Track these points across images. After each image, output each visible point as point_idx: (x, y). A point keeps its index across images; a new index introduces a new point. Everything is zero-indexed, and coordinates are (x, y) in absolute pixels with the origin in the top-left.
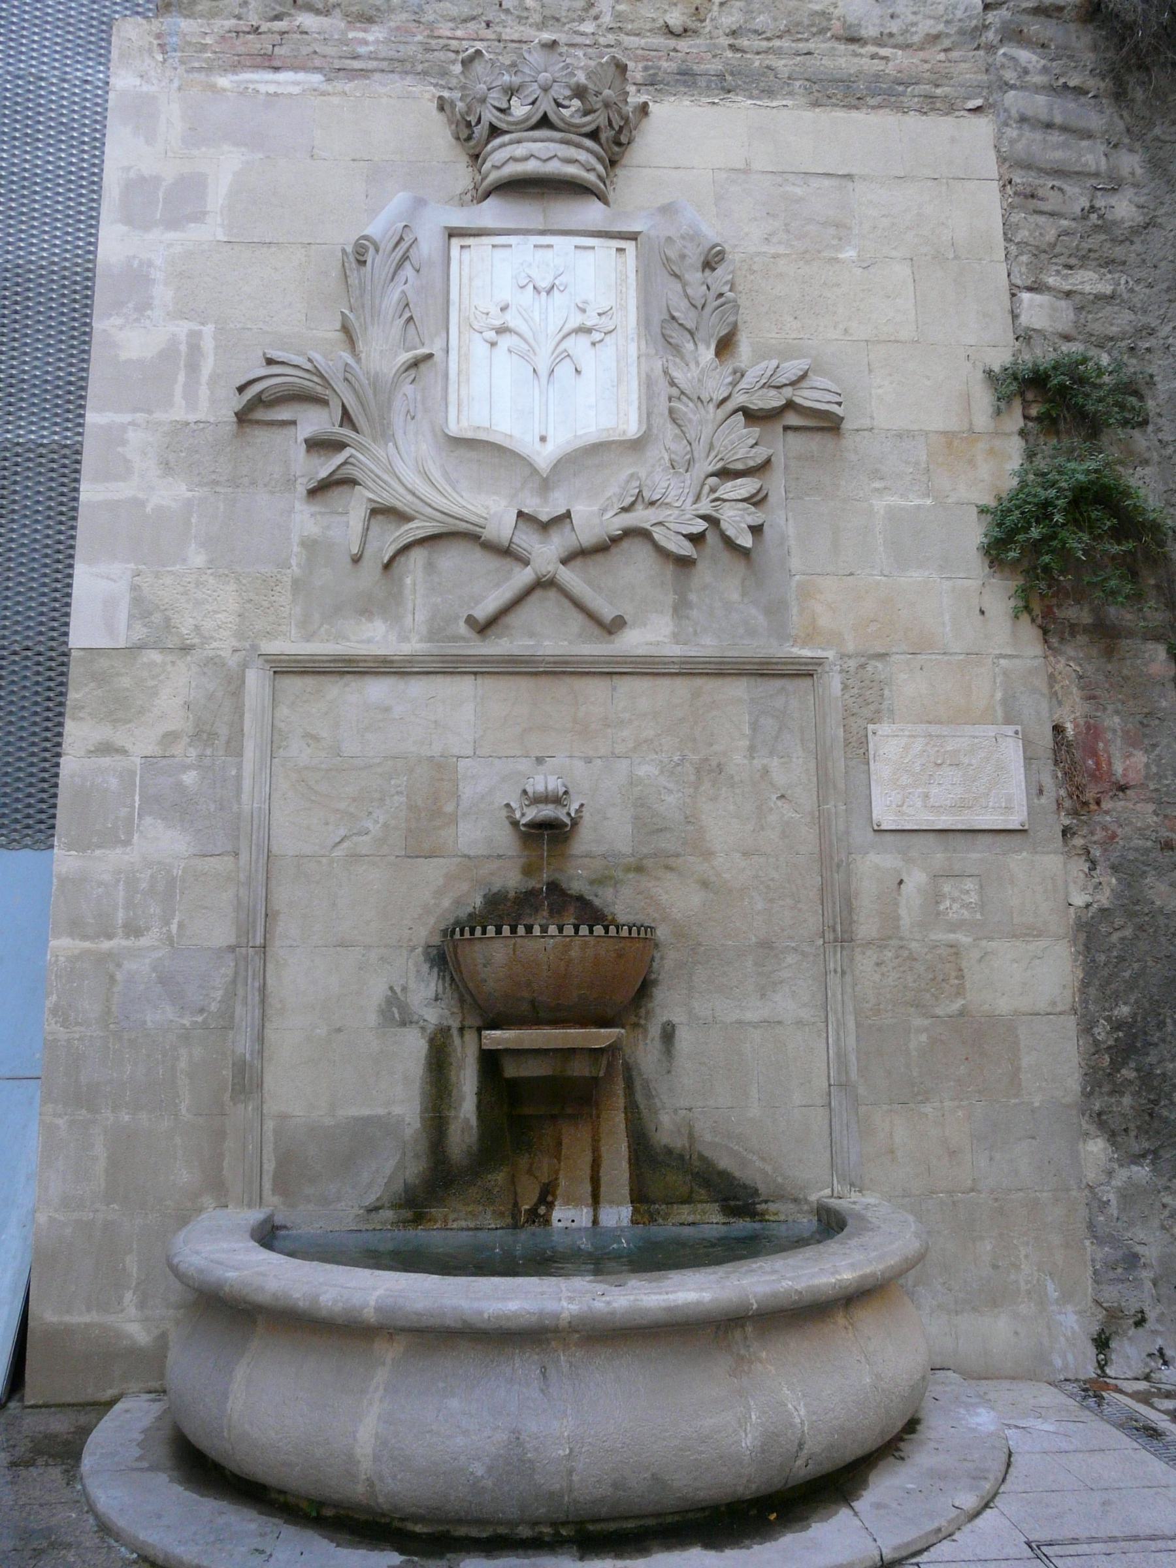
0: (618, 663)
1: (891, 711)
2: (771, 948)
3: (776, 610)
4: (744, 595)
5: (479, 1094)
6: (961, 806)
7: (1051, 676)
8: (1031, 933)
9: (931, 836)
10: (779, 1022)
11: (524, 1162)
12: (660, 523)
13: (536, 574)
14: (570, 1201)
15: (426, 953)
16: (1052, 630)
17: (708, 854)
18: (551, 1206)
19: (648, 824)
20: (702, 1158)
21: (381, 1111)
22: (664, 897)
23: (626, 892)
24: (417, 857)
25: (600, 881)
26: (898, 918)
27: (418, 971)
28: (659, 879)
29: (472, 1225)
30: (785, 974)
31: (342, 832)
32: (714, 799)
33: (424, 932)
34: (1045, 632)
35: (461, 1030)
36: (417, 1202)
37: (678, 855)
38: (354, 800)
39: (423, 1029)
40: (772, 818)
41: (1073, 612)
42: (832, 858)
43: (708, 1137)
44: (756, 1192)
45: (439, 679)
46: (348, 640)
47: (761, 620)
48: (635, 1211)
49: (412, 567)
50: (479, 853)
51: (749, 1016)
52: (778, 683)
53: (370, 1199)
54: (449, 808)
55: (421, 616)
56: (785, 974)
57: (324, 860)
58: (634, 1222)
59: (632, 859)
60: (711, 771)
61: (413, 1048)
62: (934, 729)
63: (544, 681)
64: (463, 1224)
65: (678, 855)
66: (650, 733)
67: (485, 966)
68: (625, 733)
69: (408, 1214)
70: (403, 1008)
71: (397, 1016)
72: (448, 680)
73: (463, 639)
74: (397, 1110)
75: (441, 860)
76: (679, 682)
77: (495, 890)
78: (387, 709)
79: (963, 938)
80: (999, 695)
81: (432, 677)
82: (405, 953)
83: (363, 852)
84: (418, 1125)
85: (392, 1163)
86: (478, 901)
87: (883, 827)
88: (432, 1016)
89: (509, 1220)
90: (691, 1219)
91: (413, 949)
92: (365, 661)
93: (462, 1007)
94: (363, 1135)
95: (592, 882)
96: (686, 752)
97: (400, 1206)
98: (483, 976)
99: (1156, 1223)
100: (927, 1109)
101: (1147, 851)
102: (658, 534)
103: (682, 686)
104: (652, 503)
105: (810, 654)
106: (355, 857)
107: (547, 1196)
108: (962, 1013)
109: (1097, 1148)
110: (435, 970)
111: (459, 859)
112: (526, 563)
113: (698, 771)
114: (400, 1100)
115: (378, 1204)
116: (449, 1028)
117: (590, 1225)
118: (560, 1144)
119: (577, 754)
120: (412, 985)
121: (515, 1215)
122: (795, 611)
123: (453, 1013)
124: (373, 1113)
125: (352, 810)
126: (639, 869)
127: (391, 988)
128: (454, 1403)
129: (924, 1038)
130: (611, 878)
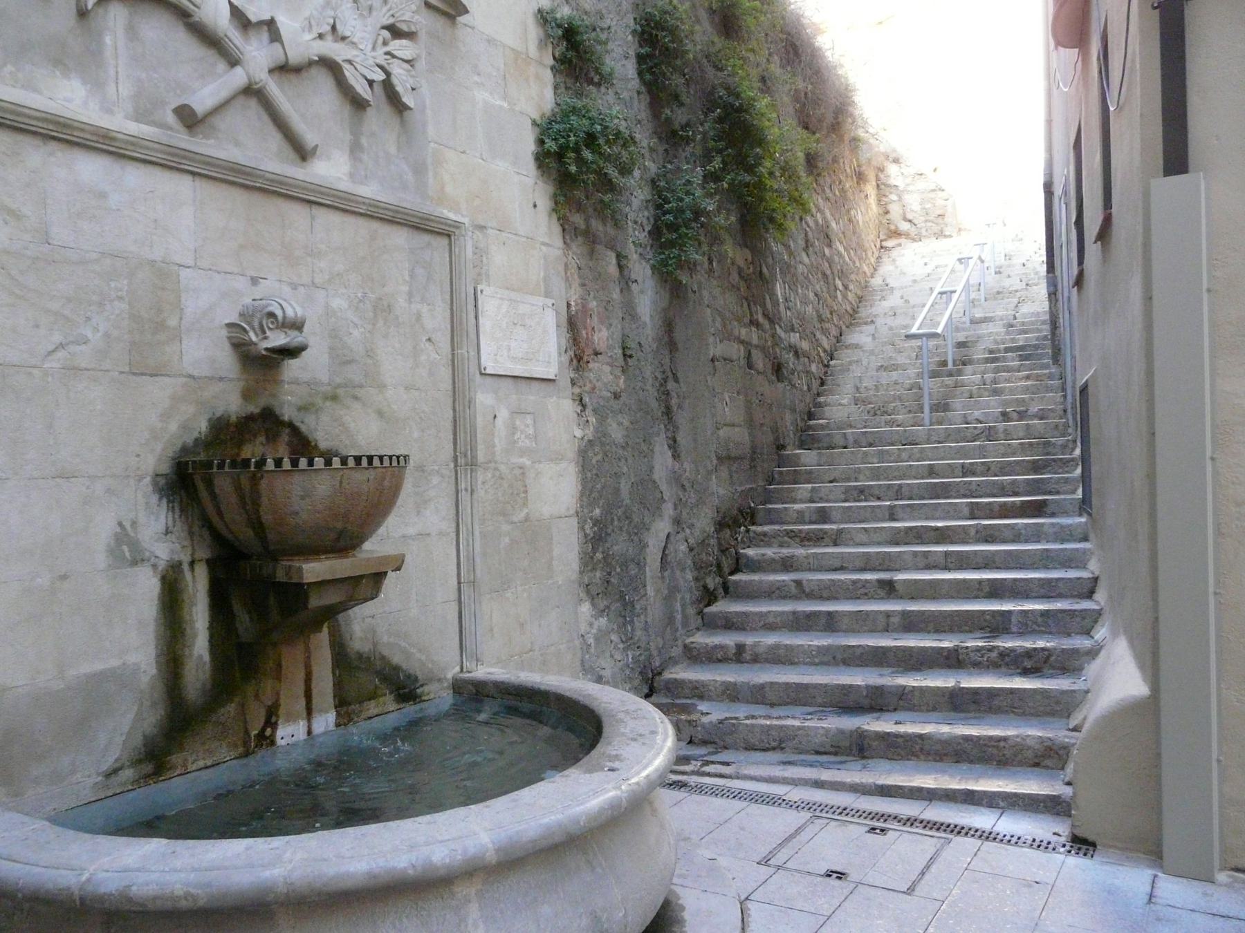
0: (322, 193)
1: (488, 276)
2: (423, 471)
3: (419, 170)
4: (399, 149)
5: (211, 628)
6: (527, 359)
7: (566, 265)
8: (558, 458)
9: (510, 381)
10: (428, 534)
11: (250, 690)
12: (350, 62)
13: (249, 79)
14: (291, 718)
15: (155, 483)
16: (568, 230)
17: (382, 387)
18: (274, 726)
19: (341, 359)
20: (383, 658)
21: (114, 663)
22: (352, 425)
23: (325, 418)
24: (142, 374)
25: (303, 408)
26: (494, 446)
27: (147, 503)
28: (348, 408)
29: (209, 764)
30: (432, 493)
31: (57, 338)
32: (386, 336)
33: (153, 458)
34: (564, 230)
35: (192, 564)
36: (155, 757)
37: (361, 386)
38: (69, 300)
39: (154, 566)
40: (423, 358)
41: (577, 219)
42: (464, 396)
43: (385, 639)
44: (416, 679)
45: (158, 173)
46: (40, 93)
47: (410, 177)
48: (338, 715)
49: (111, 24)
50: (203, 374)
51: (411, 531)
52: (426, 238)
53: (108, 763)
54: (172, 322)
55: (126, 89)
56: (432, 493)
57: (36, 372)
58: (338, 725)
59: (329, 388)
60: (383, 309)
61: (145, 588)
62: (513, 295)
63: (257, 198)
64: (201, 764)
65: (361, 386)
66: (340, 267)
67: (303, 498)
68: (322, 264)
69: (148, 768)
70: (135, 545)
71: (127, 554)
72: (167, 175)
73: (171, 129)
74: (132, 658)
75: (166, 379)
76: (361, 222)
77: (218, 414)
78: (103, 195)
79: (525, 461)
80: (542, 274)
81: (150, 168)
82: (132, 482)
83: (83, 365)
84: (154, 671)
85: (130, 716)
86: (203, 426)
87: (488, 371)
88: (163, 552)
89: (241, 749)
90: (376, 711)
91: (141, 478)
92: (82, 130)
93: (192, 540)
94: (97, 692)
95: (300, 409)
96: (367, 290)
97: (140, 761)
98: (296, 508)
99: (608, 654)
100: (509, 595)
101: (608, 400)
102: (348, 72)
103: (364, 227)
104: (344, 38)
105: (454, 218)
106: (73, 370)
107: (271, 722)
108: (527, 519)
109: (586, 608)
110: (165, 501)
111: (184, 380)
112: (233, 62)
113: (375, 308)
114: (133, 646)
115: (118, 765)
116: (180, 563)
117: (305, 737)
118: (279, 666)
119: (284, 279)
120: (142, 518)
121: (246, 744)
122: (431, 174)
123: (183, 547)
124: (107, 666)
125: (67, 312)
126: (334, 398)
127: (120, 524)
128: (546, 910)
129: (507, 540)
130: (313, 405)
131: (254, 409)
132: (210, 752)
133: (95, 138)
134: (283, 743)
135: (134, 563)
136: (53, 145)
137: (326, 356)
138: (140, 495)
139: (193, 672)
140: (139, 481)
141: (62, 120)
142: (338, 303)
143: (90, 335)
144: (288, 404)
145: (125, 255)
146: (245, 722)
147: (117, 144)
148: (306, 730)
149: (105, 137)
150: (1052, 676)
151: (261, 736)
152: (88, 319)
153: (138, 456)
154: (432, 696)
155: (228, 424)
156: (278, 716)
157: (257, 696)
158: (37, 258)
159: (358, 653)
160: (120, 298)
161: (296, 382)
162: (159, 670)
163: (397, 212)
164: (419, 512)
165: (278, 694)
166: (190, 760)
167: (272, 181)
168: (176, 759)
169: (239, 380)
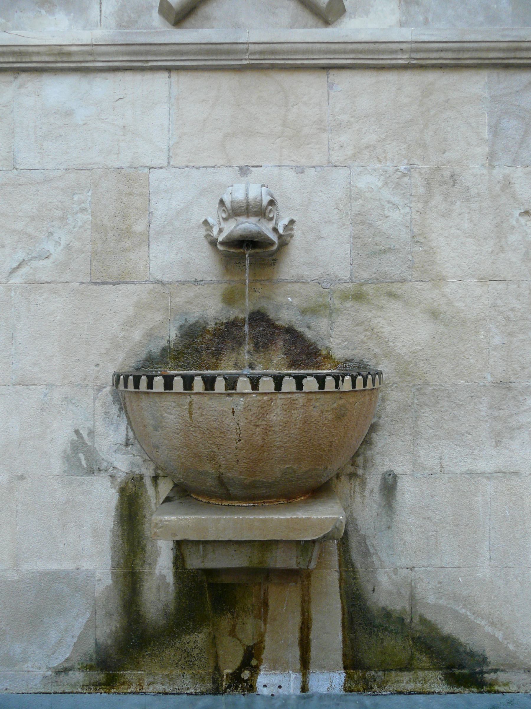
0: (335, 52)
2: (509, 388)
10: (516, 473)
14: (277, 665)
17: (438, 280)
18: (255, 671)
20: (423, 620)
21: (69, 566)
27: (106, 413)
28: (381, 308)
31: (20, 255)
32: (447, 215)
35: (155, 479)
37: (403, 281)
38: (33, 219)
39: (112, 477)
43: (431, 599)
45: (128, 77)
48: (349, 677)
51: (482, 466)
53: (58, 661)
54: (140, 227)
58: (348, 689)
59: (350, 285)
64: (160, 688)
68: (343, 138)
69: (101, 677)
70: (91, 454)
71: (84, 462)
72: (138, 77)
74: (87, 565)
75: (131, 287)
78: (69, 113)
81: (120, 76)
82: (91, 392)
83: (44, 278)
84: (110, 582)
85: (82, 621)
86: (172, 333)
88: (123, 463)
89: (210, 685)
90: (410, 687)
91: (100, 388)
94: (50, 591)
95: (304, 312)
96: (414, 160)
97: (91, 668)
106: (34, 284)
107: (251, 659)
111: (151, 286)
113: (428, 184)
115: (67, 665)
117: (298, 692)
118: (266, 604)
120: (100, 428)
124: (62, 568)
125: (30, 230)
126: (359, 297)
127: (77, 432)
130: (326, 306)
131: (240, 312)
132: (171, 679)
133: (52, 59)
134: (265, 692)
135: (91, 471)
136: (23, 77)
137: (348, 247)
138: (98, 405)
139: (154, 590)
140: (99, 390)
141: (16, 49)
142: (364, 182)
143: (52, 251)
144: (286, 310)
145: (90, 167)
146: (217, 657)
147: (73, 59)
148: (299, 685)
149: (61, 54)
150: (80, 51)
151: (236, 679)
152: (51, 234)
153: (97, 365)
154: (514, 689)
155: (204, 331)
156: (260, 662)
157: (232, 633)
158: (6, 184)
159: (384, 609)
160: (83, 210)
161: (300, 280)
162: (115, 582)
163: (459, 50)
164: (498, 443)
165: (262, 635)
166: (147, 681)
167: (261, 53)
168: (129, 674)
169: (219, 282)
